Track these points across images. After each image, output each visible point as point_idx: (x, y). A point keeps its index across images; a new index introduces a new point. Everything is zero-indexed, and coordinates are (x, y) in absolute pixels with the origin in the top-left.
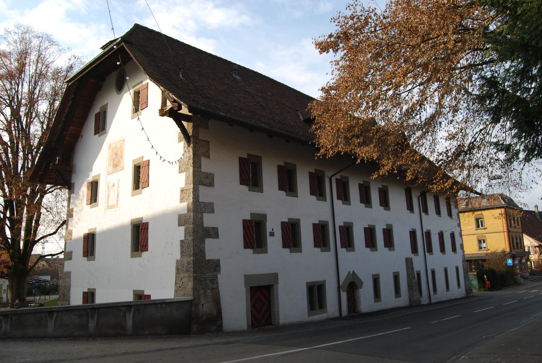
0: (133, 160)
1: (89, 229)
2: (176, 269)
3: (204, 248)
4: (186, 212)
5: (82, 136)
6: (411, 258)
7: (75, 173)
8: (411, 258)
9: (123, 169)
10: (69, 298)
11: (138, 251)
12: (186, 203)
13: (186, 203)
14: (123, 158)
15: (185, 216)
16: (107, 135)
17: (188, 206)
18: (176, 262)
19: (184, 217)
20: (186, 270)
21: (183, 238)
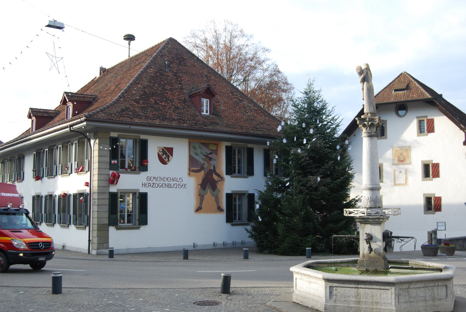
5: (355, 135)
11: (431, 210)
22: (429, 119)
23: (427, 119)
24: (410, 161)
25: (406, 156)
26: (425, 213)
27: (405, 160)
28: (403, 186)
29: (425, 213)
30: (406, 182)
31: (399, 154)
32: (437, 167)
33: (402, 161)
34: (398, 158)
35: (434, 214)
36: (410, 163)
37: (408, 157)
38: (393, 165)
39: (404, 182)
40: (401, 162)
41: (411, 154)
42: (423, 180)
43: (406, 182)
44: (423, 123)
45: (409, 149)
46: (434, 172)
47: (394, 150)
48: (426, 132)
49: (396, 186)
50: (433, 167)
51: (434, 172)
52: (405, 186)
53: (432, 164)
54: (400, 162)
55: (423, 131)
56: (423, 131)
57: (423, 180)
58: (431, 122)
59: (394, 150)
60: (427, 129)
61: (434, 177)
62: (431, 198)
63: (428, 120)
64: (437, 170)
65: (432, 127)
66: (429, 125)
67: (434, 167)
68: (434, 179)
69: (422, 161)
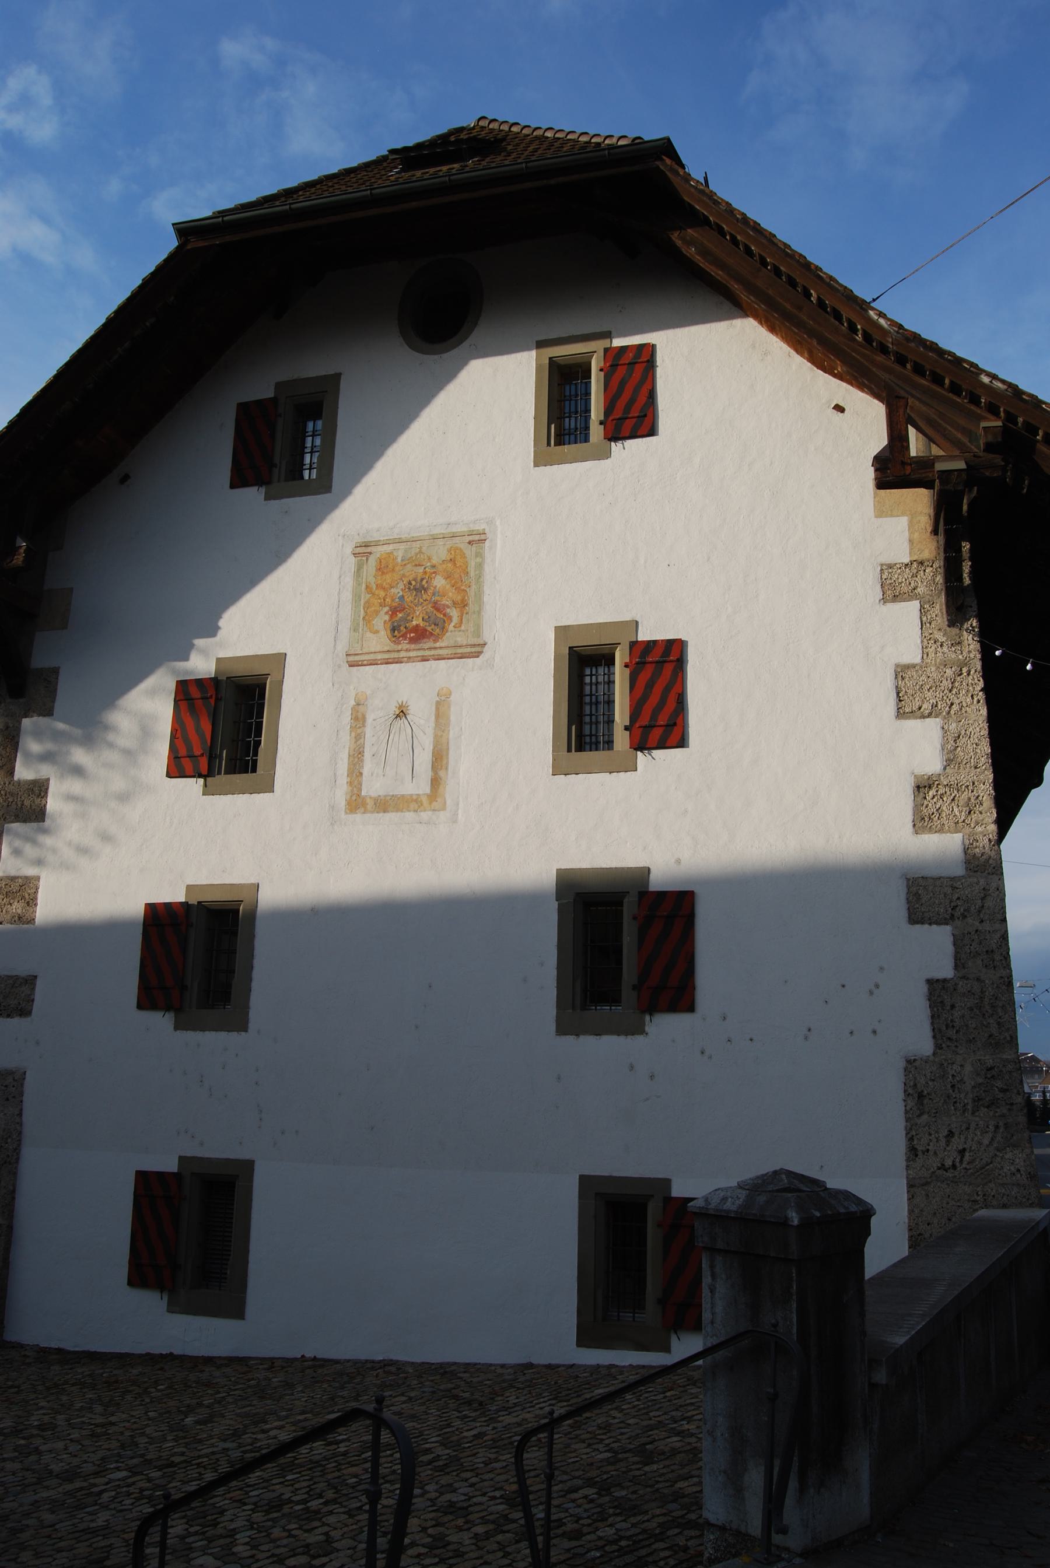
0: (687, 642)
1: (190, 888)
2: (907, 1094)
3: (662, 640)
4: (960, 871)
5: (125, 479)
6: (363, 550)
7: (64, 626)
8: (363, 550)
9: (477, 655)
10: (14, 1198)
11: (616, 1000)
12: (958, 837)
13: (958, 837)
14: (472, 607)
15: (954, 888)
16: (334, 506)
17: (966, 851)
18: (902, 1064)
19: (949, 890)
20: (977, 1100)
21: (946, 970)
22: (623, 349)
23: (606, 350)
24: (478, 631)
25: (445, 601)
26: (563, 1028)
27: (444, 629)
28: (409, 816)
29: (563, 1028)
30: (436, 782)
31: (397, 591)
32: (668, 669)
33: (419, 635)
34: (394, 611)
35: (639, 1030)
36: (476, 651)
37: (462, 605)
38: (350, 666)
39: (421, 786)
40: (412, 641)
41: (487, 590)
42: (558, 769)
43: (436, 782)
44: (591, 675)
45: (470, 551)
46: (621, 404)
47: (372, 561)
48: (621, 739)
49: (358, 817)
50: (635, 669)
51: (621, 404)
52: (425, 815)
53: (634, 644)
54: (404, 644)
55: (591, 743)
56: (591, 743)
57: (558, 769)
58: (632, 364)
59: (372, 561)
60: (634, 715)
61: (642, 744)
62: (603, 658)
63: (615, 358)
64: (667, 690)
65: (642, 399)
66: (622, 384)
67: (649, 670)
68: (616, 447)
69: (561, 632)
